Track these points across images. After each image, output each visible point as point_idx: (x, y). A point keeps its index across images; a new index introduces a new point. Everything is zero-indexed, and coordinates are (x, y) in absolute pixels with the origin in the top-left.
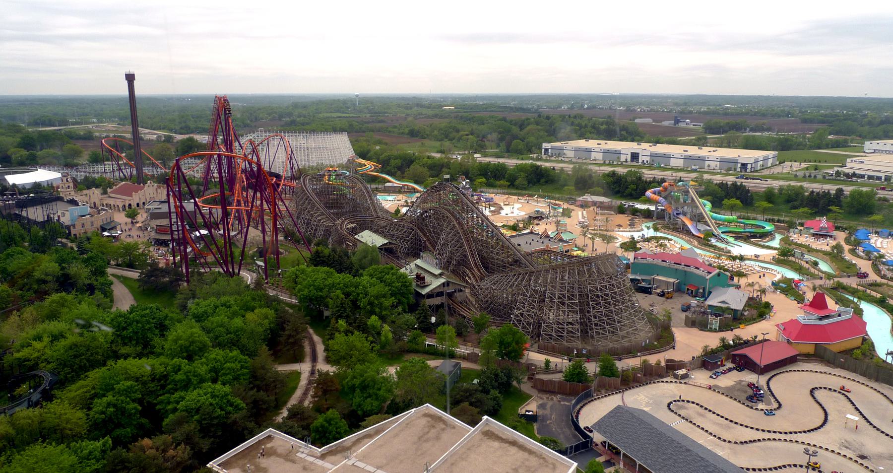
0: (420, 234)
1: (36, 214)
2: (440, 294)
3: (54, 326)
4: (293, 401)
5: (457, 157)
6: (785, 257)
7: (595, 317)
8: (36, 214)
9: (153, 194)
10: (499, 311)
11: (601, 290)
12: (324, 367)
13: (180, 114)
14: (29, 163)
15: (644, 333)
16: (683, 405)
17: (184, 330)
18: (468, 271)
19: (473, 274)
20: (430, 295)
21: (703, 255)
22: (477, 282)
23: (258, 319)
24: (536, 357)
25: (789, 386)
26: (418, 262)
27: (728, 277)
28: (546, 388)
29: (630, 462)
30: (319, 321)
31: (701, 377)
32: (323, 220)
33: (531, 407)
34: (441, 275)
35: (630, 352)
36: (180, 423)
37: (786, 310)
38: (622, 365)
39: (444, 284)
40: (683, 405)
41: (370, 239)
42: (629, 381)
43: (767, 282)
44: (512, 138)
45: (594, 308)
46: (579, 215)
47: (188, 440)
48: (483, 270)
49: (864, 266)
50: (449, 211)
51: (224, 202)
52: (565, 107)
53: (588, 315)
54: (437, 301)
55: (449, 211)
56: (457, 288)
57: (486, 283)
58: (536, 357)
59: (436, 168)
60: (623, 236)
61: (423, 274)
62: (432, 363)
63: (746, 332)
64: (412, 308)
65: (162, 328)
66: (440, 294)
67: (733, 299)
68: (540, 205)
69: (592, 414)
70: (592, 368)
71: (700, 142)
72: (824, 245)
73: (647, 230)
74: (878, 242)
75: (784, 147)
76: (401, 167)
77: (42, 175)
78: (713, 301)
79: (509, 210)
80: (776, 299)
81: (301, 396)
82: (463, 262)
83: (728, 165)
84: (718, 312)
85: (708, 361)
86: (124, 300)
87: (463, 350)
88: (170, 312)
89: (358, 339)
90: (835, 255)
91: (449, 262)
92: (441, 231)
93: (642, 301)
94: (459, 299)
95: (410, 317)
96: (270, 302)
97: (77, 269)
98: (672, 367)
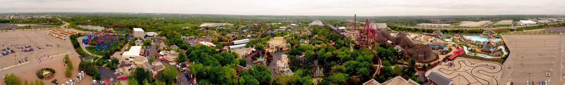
1: (342, 33)
3: (343, 53)
4: (376, 73)
5: (403, 27)
6: (453, 41)
8: (342, 33)
9: (357, 32)
10: (411, 55)
12: (382, 66)
13: (361, 19)
14: (341, 26)
15: (434, 57)
16: (440, 70)
17: (360, 57)
21: (442, 42)
23: (371, 57)
24: (417, 64)
25: (455, 62)
27: (446, 45)
28: (419, 70)
29: (434, 83)
30: (381, 58)
31: (443, 63)
32: (382, 38)
33: (417, 74)
35: (432, 61)
36: (359, 74)
37: (454, 49)
38: (431, 64)
40: (440, 70)
41: (390, 42)
42: (433, 66)
43: (451, 45)
44: (412, 23)
46: (423, 36)
47: (360, 78)
49: (463, 40)
51: (367, 34)
57: (409, 50)
58: (417, 64)
59: (400, 29)
60: (430, 40)
62: (399, 66)
63: (449, 54)
64: (396, 55)
65: (357, 56)
67: (446, 49)
68: (417, 35)
69: (427, 74)
70: (427, 65)
71: (440, 23)
72: (458, 38)
73: (434, 38)
74: (464, 36)
75: (452, 23)
76: (394, 29)
77: (343, 28)
78: (444, 50)
79: (411, 36)
80: (453, 48)
81: (377, 72)
82: (405, 46)
83: (445, 27)
84: (445, 51)
85: (444, 60)
86: (352, 50)
87: (405, 63)
88: (358, 53)
89: (387, 62)
90: (459, 39)
93: (434, 51)
95: (396, 57)
96: (373, 53)
97: (346, 43)
98: (439, 62)
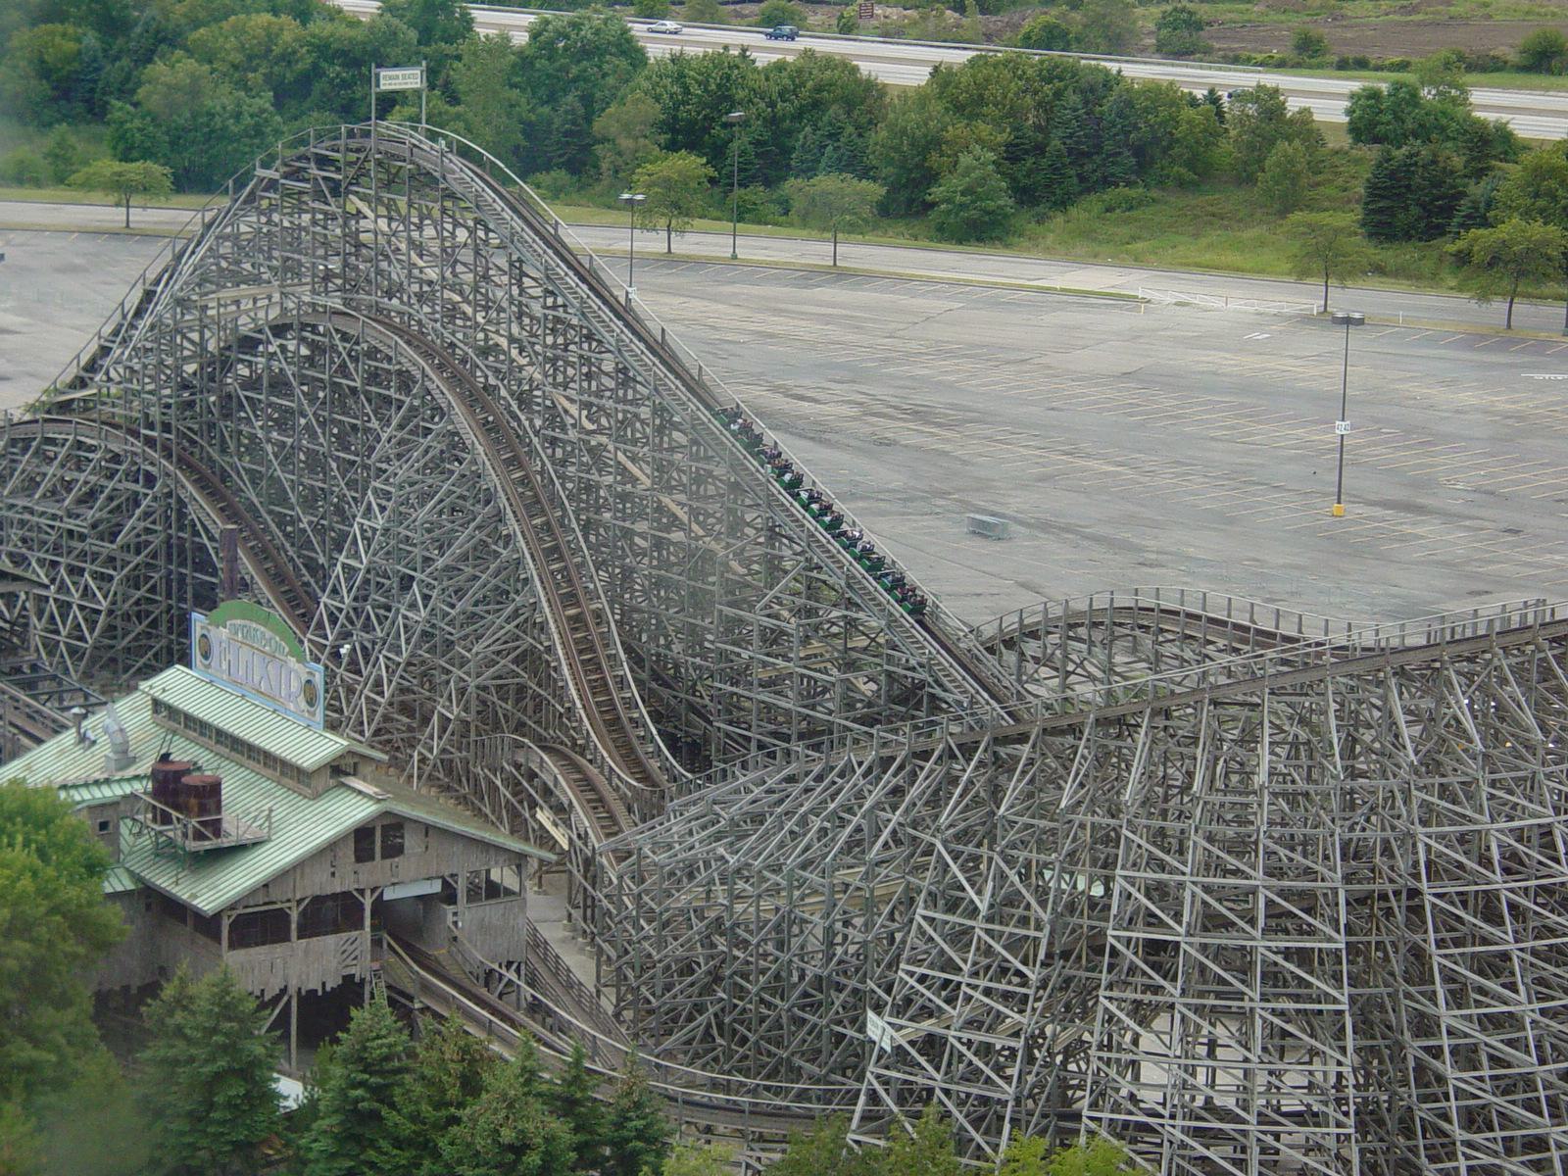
0: (201, 508)
2: (331, 914)
7: (1466, 1057)
11: (1513, 865)
18: (551, 769)
19: (586, 784)
20: (258, 923)
22: (611, 826)
26: (175, 684)
34: (338, 770)
39: (362, 836)
45: (1457, 998)
48: (659, 756)
50: (417, 341)
52: (40, 803)
53: (1414, 1047)
54: (311, 963)
55: (443, 359)
56: (463, 867)
57: (678, 832)
61: (205, 760)
66: (331, 914)
82: (521, 702)
91: (413, 710)
92: (358, 486)
94: (479, 955)
